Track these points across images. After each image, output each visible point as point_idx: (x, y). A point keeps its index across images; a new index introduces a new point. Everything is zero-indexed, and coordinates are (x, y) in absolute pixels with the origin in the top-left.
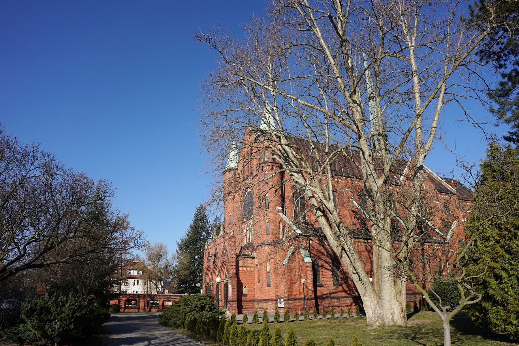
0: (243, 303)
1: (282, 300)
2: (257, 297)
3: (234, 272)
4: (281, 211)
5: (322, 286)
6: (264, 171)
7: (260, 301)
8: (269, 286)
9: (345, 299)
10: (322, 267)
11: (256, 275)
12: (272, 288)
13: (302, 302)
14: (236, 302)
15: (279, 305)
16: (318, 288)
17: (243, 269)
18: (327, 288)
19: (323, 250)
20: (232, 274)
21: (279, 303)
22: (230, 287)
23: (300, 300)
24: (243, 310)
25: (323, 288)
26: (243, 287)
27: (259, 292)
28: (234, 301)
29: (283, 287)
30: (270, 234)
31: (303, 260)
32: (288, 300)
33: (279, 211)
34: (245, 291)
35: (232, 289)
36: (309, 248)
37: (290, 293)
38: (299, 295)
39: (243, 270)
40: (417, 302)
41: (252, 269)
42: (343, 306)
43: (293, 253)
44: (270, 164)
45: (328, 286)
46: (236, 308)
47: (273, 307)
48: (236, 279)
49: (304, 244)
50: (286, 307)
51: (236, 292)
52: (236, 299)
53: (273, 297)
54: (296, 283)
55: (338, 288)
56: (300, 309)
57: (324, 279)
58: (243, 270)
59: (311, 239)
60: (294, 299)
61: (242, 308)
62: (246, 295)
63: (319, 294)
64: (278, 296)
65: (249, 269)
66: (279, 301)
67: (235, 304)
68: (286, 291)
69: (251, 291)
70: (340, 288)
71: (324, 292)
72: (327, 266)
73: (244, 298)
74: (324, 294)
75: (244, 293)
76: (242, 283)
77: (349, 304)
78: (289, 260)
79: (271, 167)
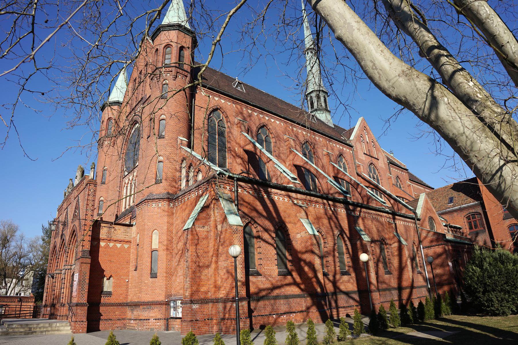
0: (102, 309)
1: (179, 303)
2: (132, 298)
3: (87, 246)
4: (186, 143)
5: (258, 274)
6: (162, 80)
7: (136, 305)
8: (154, 276)
9: (298, 300)
10: (259, 237)
11: (132, 257)
12: (160, 281)
13: (220, 306)
14: (86, 308)
15: (173, 314)
16: (251, 278)
17: (115, 245)
18: (267, 279)
19: (260, 208)
20: (83, 251)
21: (172, 309)
22: (76, 278)
23: (217, 302)
24: (101, 322)
25: (260, 278)
26: (105, 279)
27: (136, 287)
28: (82, 305)
29: (182, 277)
30: (163, 181)
31: (225, 219)
32: (192, 302)
33: (182, 144)
34: (108, 285)
35: (80, 280)
36: (237, 201)
37: (194, 288)
38: (215, 292)
39: (107, 246)
40: (395, 302)
41: (126, 246)
42: (294, 312)
43: (205, 208)
44: (173, 69)
45: (270, 276)
46: (85, 319)
47: (159, 317)
48: (89, 261)
49: (226, 192)
50: (186, 319)
51: (86, 287)
52: (85, 302)
53: (161, 298)
54: (208, 267)
55: (285, 279)
56: (215, 321)
57: (261, 262)
58: (107, 246)
59: (241, 186)
60: (204, 301)
61: (100, 319)
62: (109, 294)
63: (252, 289)
64: (171, 295)
65: (119, 245)
66: (172, 304)
67: (82, 313)
68: (188, 284)
69: (120, 286)
70: (289, 279)
71: (262, 286)
72: (266, 236)
73: (104, 300)
74: (261, 290)
75: (105, 289)
76: (103, 271)
77: (304, 309)
78: (197, 219)
79: (174, 73)
